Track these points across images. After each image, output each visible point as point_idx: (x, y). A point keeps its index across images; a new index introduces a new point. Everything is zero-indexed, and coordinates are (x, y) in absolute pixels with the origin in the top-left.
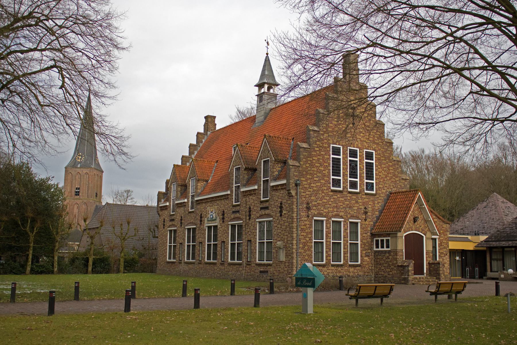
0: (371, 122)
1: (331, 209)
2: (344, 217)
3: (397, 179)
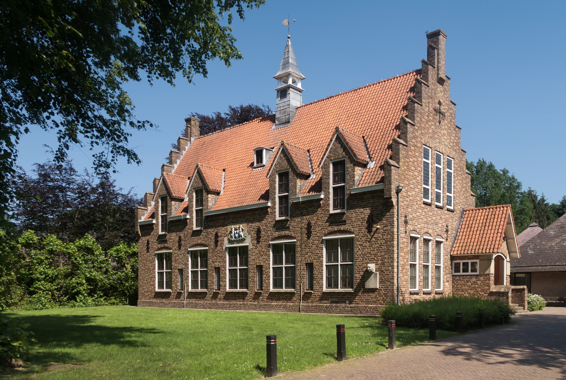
0: (452, 123)
1: (423, 225)
2: (432, 235)
3: (468, 194)
